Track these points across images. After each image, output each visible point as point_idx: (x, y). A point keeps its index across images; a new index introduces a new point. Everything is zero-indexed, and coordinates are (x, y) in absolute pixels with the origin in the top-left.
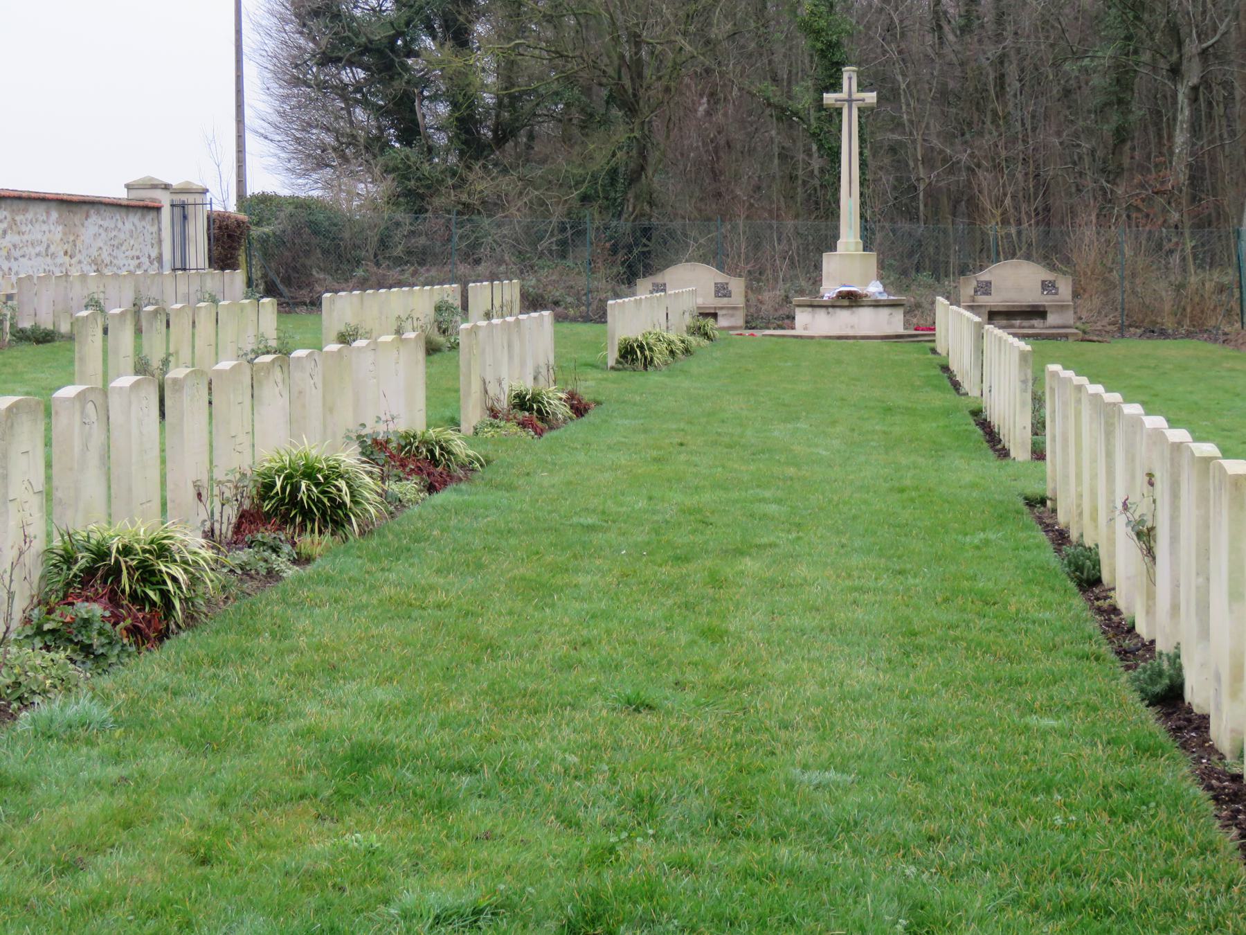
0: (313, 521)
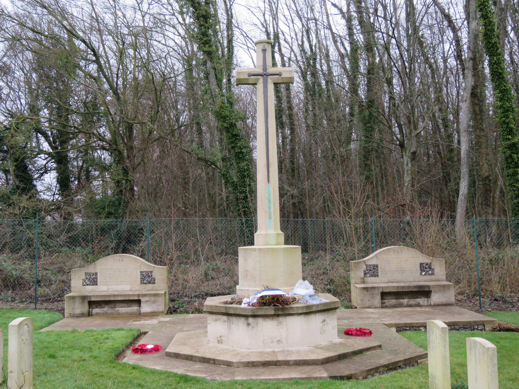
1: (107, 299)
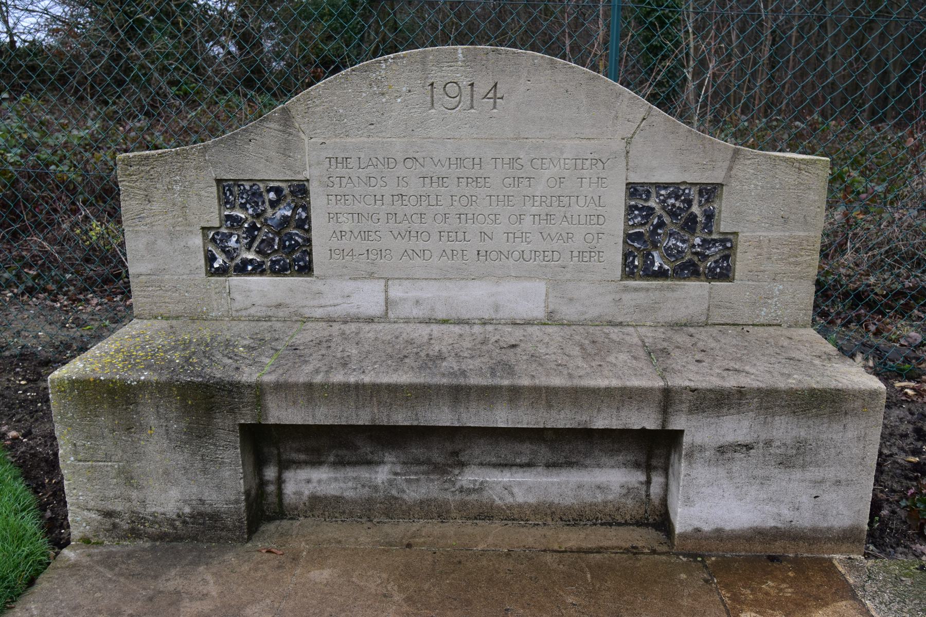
1: (401, 418)
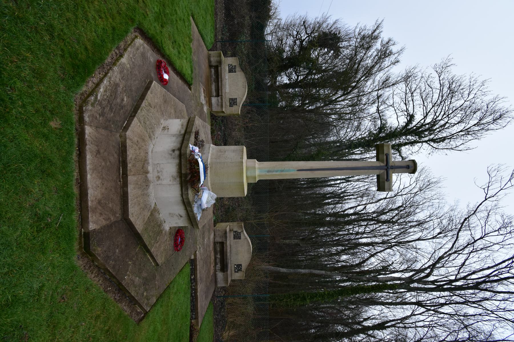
0: (319, 257)
1: (219, 77)
